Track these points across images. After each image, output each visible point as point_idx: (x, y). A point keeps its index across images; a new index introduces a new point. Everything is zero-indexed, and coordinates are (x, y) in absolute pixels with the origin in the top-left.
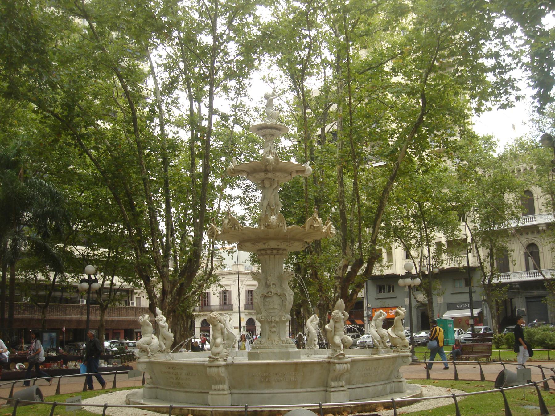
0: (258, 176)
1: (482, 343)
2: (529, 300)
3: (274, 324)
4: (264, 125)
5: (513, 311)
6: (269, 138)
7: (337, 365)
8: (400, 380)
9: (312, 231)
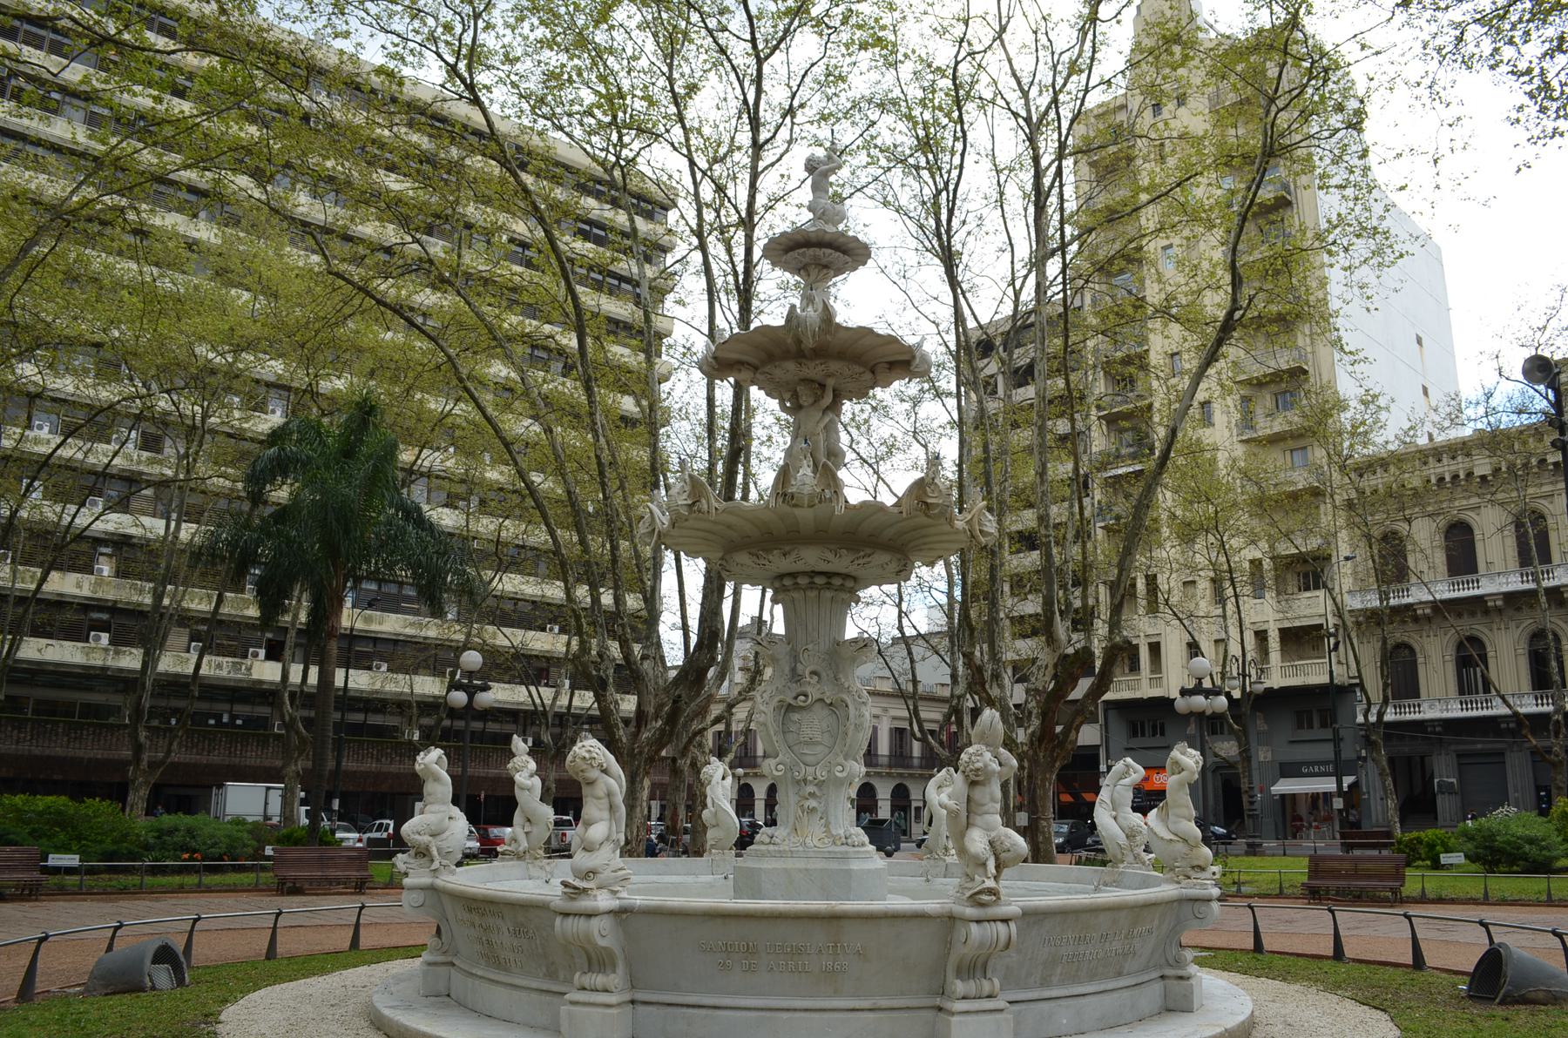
0: (778, 373)
1: (1375, 853)
2: (1465, 760)
3: (811, 789)
4: (799, 237)
6: (814, 272)
7: (974, 927)
8: (1180, 973)
9: (923, 520)
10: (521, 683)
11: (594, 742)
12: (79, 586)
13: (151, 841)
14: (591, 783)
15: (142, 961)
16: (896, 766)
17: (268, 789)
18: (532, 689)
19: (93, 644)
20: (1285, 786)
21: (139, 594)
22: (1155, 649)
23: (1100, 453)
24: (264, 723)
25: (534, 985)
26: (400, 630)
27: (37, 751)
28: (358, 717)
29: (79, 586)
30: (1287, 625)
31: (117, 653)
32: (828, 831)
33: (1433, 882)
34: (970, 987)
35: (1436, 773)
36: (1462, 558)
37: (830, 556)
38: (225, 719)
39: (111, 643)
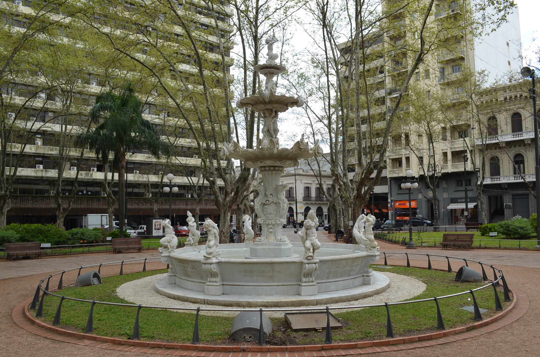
3: (271, 226)
5: (502, 205)
6: (269, 75)
7: (307, 265)
9: (299, 152)
10: (186, 176)
11: (210, 220)
12: (31, 149)
13: (70, 237)
14: (210, 231)
15: (90, 278)
16: (318, 201)
17: (102, 216)
18: (189, 178)
19: (37, 169)
20: (452, 206)
21: (54, 151)
22: (408, 159)
23: (389, 88)
24: (98, 193)
25: (198, 281)
26: (142, 159)
27: (23, 206)
28: (130, 190)
29: (31, 149)
30: (454, 150)
31: (46, 171)
32: (276, 238)
33: (485, 241)
34: (307, 280)
35: (505, 201)
36: (517, 126)
37: (274, 162)
38: (85, 192)
39: (44, 168)
